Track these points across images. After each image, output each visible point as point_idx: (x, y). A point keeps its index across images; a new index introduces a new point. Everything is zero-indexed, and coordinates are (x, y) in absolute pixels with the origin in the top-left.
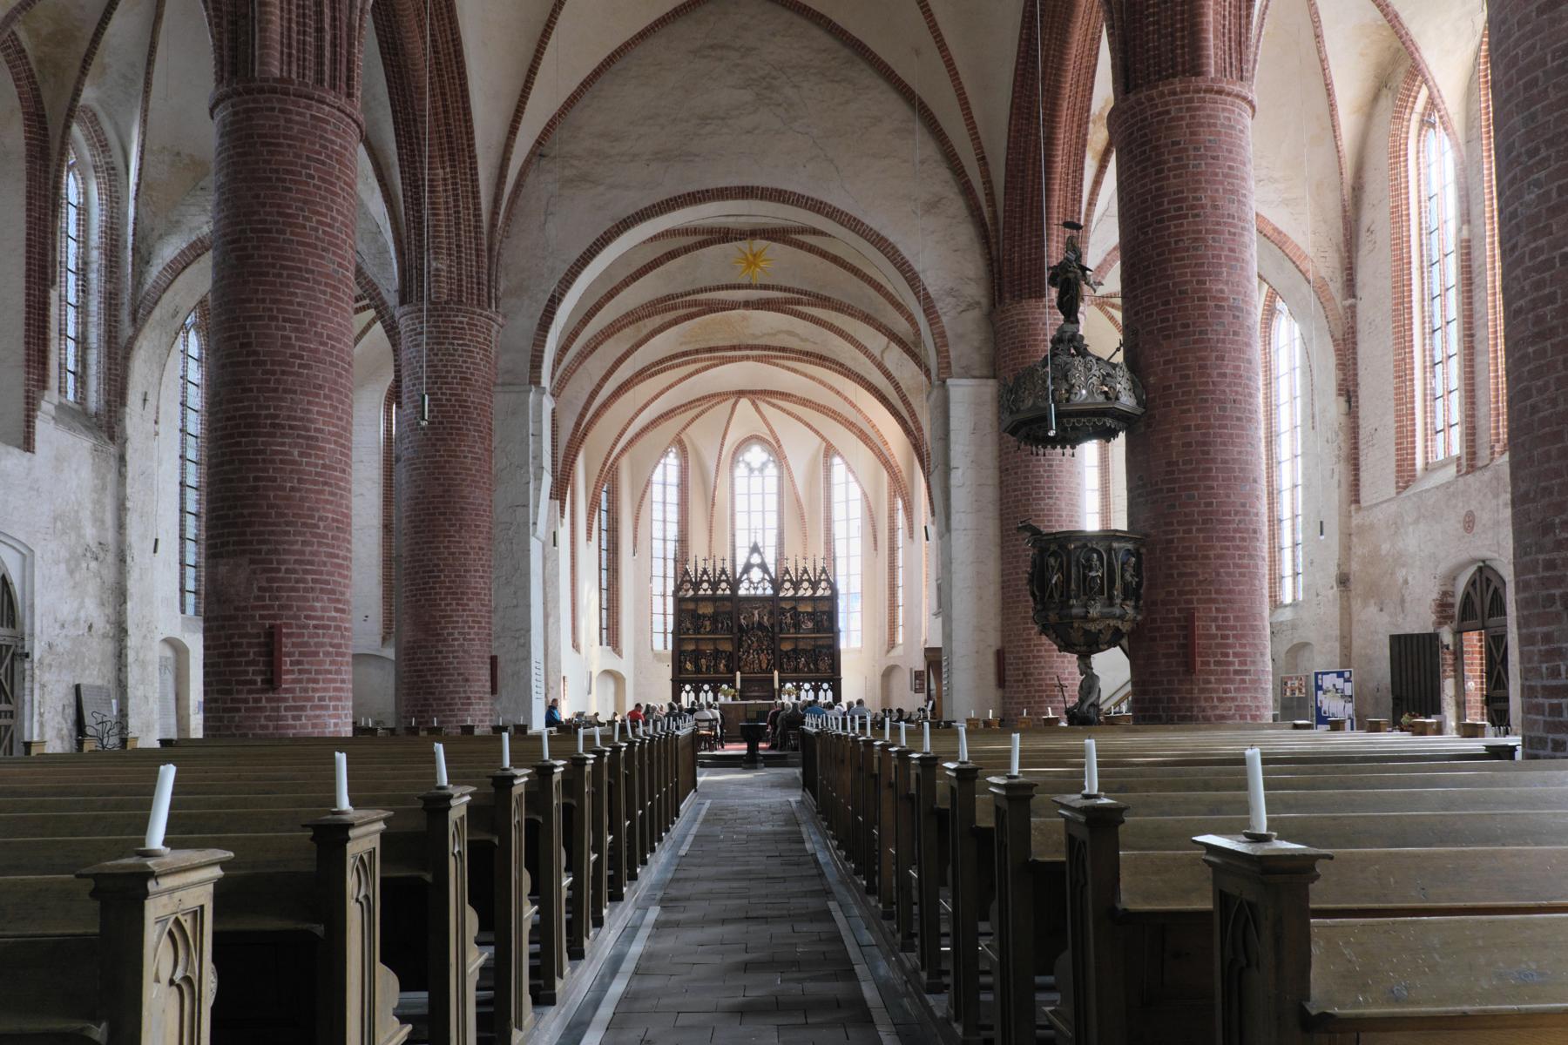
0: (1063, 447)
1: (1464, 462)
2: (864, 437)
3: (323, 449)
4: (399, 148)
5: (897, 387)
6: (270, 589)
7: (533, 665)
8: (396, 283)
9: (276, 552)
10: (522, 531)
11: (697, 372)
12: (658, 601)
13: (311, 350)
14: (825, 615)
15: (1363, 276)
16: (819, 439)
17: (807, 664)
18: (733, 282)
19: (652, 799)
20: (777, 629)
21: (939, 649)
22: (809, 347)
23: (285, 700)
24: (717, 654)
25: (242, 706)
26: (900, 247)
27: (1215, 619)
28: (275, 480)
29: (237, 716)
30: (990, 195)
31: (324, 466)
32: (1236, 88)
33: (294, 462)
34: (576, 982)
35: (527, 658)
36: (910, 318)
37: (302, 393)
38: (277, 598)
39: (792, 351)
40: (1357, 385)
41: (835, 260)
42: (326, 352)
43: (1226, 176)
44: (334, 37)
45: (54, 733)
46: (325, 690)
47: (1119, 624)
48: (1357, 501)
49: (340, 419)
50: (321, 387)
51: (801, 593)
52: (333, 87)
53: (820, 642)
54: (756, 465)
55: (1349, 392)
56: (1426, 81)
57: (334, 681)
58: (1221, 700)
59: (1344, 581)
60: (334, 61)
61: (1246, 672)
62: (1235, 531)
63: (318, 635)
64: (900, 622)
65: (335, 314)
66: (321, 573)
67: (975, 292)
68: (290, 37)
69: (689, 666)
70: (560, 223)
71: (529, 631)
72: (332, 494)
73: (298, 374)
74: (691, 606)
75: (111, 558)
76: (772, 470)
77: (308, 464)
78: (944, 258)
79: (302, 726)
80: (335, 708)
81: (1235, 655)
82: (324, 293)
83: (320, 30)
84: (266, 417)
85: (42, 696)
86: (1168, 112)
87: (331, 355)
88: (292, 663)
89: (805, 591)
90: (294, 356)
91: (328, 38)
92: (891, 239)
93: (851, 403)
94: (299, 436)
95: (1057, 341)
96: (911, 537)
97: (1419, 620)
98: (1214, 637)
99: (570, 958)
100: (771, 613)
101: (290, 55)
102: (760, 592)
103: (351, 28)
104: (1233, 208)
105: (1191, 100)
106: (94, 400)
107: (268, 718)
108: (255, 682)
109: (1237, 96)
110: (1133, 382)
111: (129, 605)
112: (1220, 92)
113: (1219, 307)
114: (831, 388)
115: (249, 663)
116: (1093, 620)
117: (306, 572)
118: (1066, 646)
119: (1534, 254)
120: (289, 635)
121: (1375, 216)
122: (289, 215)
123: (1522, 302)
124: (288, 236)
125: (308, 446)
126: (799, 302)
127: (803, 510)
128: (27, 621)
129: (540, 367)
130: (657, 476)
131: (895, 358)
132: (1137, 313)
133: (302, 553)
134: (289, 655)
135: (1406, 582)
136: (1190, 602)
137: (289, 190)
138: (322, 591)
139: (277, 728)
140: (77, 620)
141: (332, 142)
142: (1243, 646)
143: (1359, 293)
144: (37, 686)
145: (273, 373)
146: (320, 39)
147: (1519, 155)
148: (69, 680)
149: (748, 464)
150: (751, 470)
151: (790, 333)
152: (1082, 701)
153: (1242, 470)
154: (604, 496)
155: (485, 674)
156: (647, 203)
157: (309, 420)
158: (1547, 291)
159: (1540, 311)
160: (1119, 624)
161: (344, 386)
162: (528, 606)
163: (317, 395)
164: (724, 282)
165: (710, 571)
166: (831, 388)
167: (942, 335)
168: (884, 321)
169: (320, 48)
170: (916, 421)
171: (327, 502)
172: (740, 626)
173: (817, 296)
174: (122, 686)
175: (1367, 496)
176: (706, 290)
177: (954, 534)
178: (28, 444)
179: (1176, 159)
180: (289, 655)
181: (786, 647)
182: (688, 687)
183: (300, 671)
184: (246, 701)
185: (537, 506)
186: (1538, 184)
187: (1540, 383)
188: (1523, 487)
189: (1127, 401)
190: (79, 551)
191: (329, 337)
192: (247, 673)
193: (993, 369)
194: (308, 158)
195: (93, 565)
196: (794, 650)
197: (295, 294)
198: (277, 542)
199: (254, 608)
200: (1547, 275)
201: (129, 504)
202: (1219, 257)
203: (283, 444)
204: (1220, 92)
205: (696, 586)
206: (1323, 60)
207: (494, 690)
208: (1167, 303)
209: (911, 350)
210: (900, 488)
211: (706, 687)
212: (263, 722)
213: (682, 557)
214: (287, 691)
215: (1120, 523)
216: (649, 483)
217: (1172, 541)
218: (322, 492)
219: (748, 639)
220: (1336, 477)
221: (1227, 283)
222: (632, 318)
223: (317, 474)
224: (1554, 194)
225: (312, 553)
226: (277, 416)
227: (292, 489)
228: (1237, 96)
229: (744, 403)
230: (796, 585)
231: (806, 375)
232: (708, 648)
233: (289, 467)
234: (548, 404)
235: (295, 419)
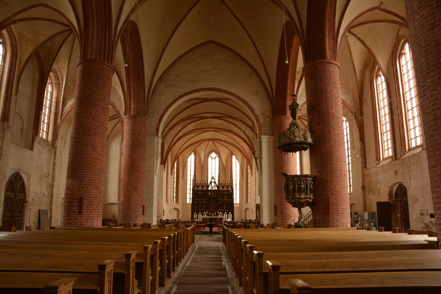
0: (293, 152)
1: (394, 157)
2: (240, 150)
3: (98, 150)
4: (126, 78)
5: (248, 138)
6: (81, 187)
7: (154, 207)
8: (124, 111)
9: (84, 177)
10: (152, 173)
11: (199, 134)
12: (188, 191)
13: (96, 125)
14: (230, 195)
15: (364, 111)
16: (229, 151)
17: (225, 207)
19: (177, 250)
21: (259, 204)
22: (226, 128)
23: (84, 217)
25: (72, 218)
26: (249, 103)
27: (335, 199)
28: (84, 158)
29: (71, 221)
30: (271, 87)
31: (98, 155)
32: (335, 62)
33: (90, 154)
34: (169, 283)
35: (152, 206)
36: (252, 121)
37: (94, 136)
38: (83, 190)
39: (222, 129)
40: (364, 138)
41: (234, 107)
42: (100, 126)
43: (333, 83)
44: (109, 49)
45: (32, 222)
46: (95, 214)
47: (309, 200)
48: (366, 167)
49: (103, 143)
50: (98, 134)
51: (224, 189)
52: (107, 61)
54: (214, 157)
55: (362, 139)
56: (378, 64)
57: (97, 212)
58: (337, 221)
59: (363, 188)
60: (108, 55)
61: (344, 213)
62: (339, 175)
63: (93, 200)
65: (103, 116)
66: (95, 183)
67: (268, 114)
68: (98, 49)
69: (196, 207)
70: (165, 97)
71: (153, 198)
72: (99, 162)
73: (93, 131)
74: (197, 192)
75: (51, 177)
76: (217, 159)
77: (94, 154)
78: (258, 106)
79: (88, 224)
80: (97, 219)
81: (341, 209)
82: (101, 110)
83: (105, 47)
84: (84, 142)
85: (30, 212)
86: (318, 68)
87: (102, 126)
88: (86, 207)
89: (225, 189)
90: (92, 126)
91: (107, 49)
92: (247, 101)
93: (237, 142)
94: (92, 147)
95: (291, 125)
96: (252, 175)
97: (385, 198)
98: (334, 204)
99: (168, 277)
100: (216, 194)
101: (97, 53)
102: (214, 189)
103: (113, 47)
104: (335, 92)
105: (324, 65)
106: (50, 139)
107: (79, 222)
108: (76, 212)
109: (335, 64)
110: (311, 135)
111: (54, 189)
112: (331, 63)
113: (333, 116)
114: (232, 138)
115: (75, 207)
116: (302, 199)
117: (91, 182)
118: (294, 205)
119: (431, 96)
120: (86, 199)
121: (367, 96)
122: (94, 91)
123: (429, 110)
124: (93, 96)
125: (94, 150)
126: (224, 117)
127: (225, 169)
128: (28, 193)
129: (158, 131)
130: (189, 160)
131: (248, 131)
132: (311, 118)
133: (91, 177)
134: (86, 205)
135: (380, 188)
136: (328, 194)
137: (94, 85)
138: (95, 188)
139: (81, 224)
140: (40, 193)
141: (106, 74)
142: (343, 206)
143: (364, 115)
144: (29, 210)
145: (86, 130)
146: (105, 49)
147: (424, 70)
148: (37, 208)
149: (212, 157)
150: (212, 158)
151: (222, 125)
152: (299, 221)
153: (340, 159)
154: (175, 164)
155: (141, 209)
156: (187, 91)
157: (95, 143)
158: (437, 107)
159: (435, 112)
160: (309, 200)
161: (104, 134)
162: (153, 192)
163: (97, 136)
164: (206, 112)
165: (202, 183)
166: (232, 138)
167: (260, 125)
168: (245, 122)
169: (105, 52)
170: (253, 147)
171: (98, 164)
173: (229, 115)
174: (51, 210)
175: (368, 166)
176: (201, 114)
177: (263, 175)
178: (32, 149)
179: (320, 79)
180: (86, 205)
181: (220, 203)
182: (195, 213)
183: (88, 209)
184: (73, 217)
185: (156, 166)
186: (431, 77)
187: (437, 133)
188: (433, 163)
189: (310, 140)
190: (43, 175)
191: (101, 122)
192: (74, 209)
193: (272, 133)
194: (100, 78)
195: (46, 179)
196: (222, 204)
197: (93, 111)
198: (84, 175)
199: (77, 192)
200: (436, 102)
201: (56, 164)
202: (332, 103)
203: (87, 149)
204: (331, 63)
205: (198, 187)
206: (352, 60)
207: (143, 214)
208: (319, 115)
209: (252, 129)
210: (249, 163)
212: (77, 223)
213: (194, 180)
214: (84, 214)
215: (307, 171)
216: (187, 161)
217: (323, 178)
218: (97, 161)
219: (212, 200)
220: (360, 161)
221: (335, 110)
222: (183, 120)
223: (96, 157)
224: (437, 79)
225: (93, 178)
226: (86, 142)
227: (89, 161)
228: (335, 64)
229: (211, 142)
230: (223, 187)
231: (226, 135)
233: (88, 155)
234: (160, 141)
235: (91, 142)
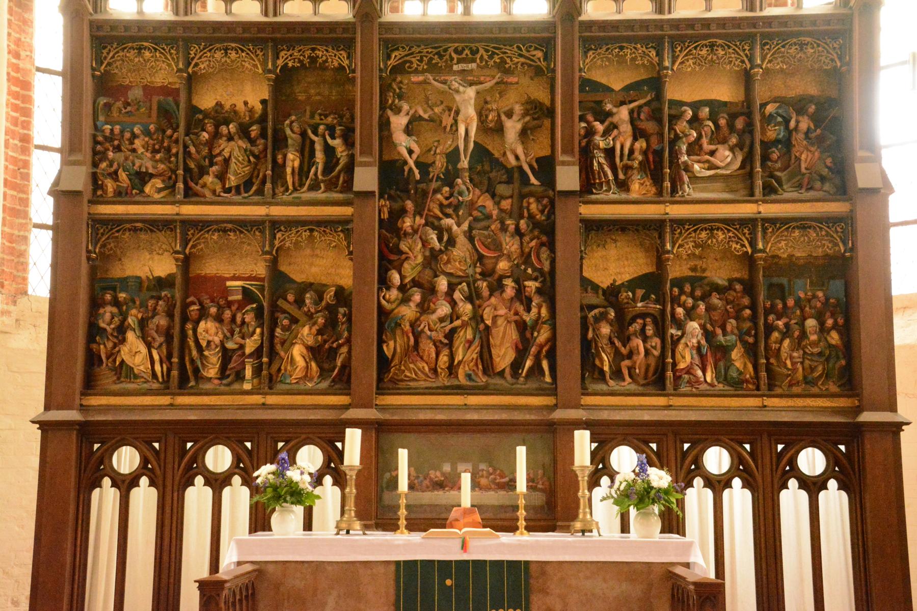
18: (579, 268)
20: (568, 177)
24: (275, 302)
53: (783, 247)
64: (67, 584)
69: (135, 352)
74: (164, 72)
100: (539, 113)
172: (392, 173)
181: (614, 265)
196: (651, 283)
211: (219, 458)
232: (237, 267)
